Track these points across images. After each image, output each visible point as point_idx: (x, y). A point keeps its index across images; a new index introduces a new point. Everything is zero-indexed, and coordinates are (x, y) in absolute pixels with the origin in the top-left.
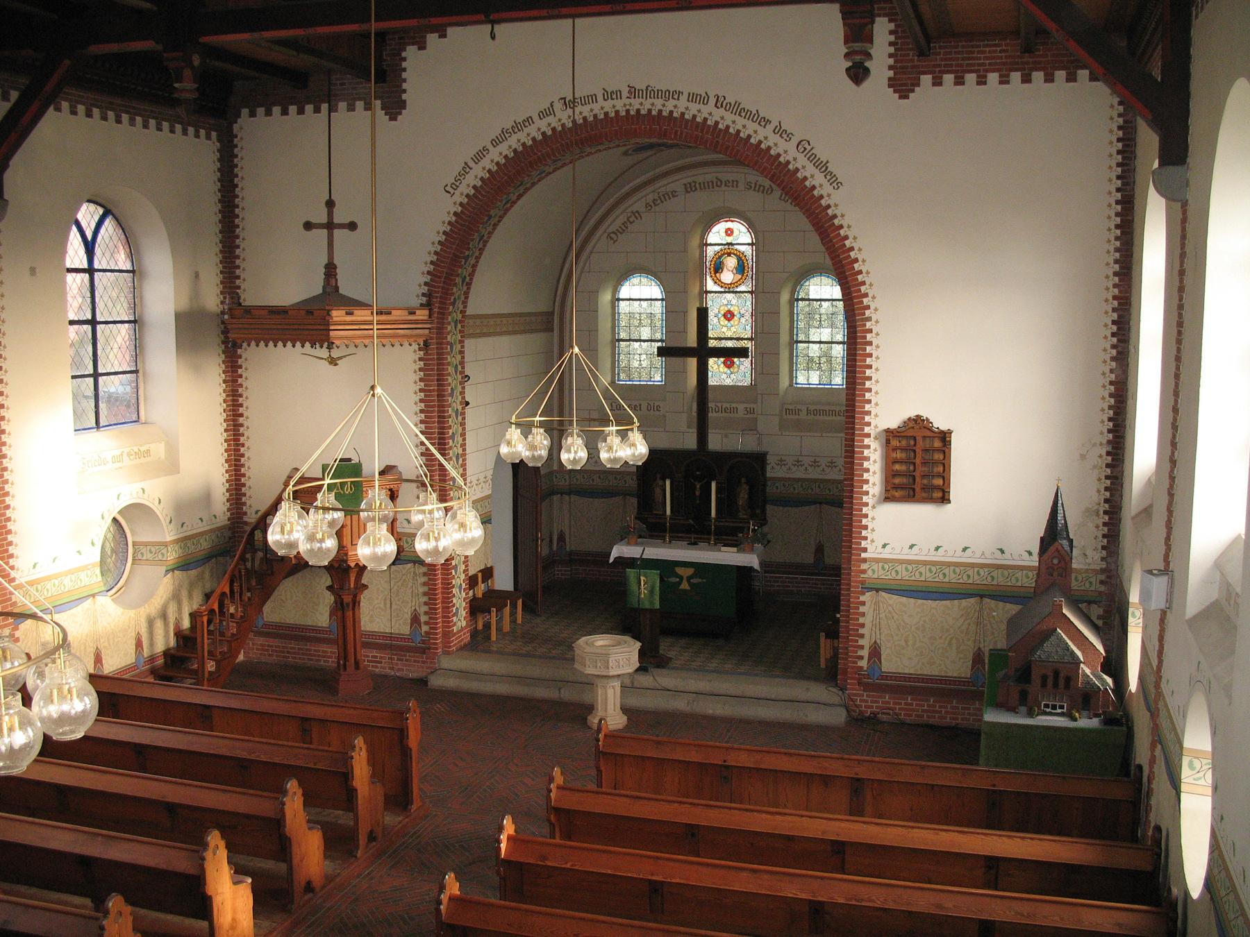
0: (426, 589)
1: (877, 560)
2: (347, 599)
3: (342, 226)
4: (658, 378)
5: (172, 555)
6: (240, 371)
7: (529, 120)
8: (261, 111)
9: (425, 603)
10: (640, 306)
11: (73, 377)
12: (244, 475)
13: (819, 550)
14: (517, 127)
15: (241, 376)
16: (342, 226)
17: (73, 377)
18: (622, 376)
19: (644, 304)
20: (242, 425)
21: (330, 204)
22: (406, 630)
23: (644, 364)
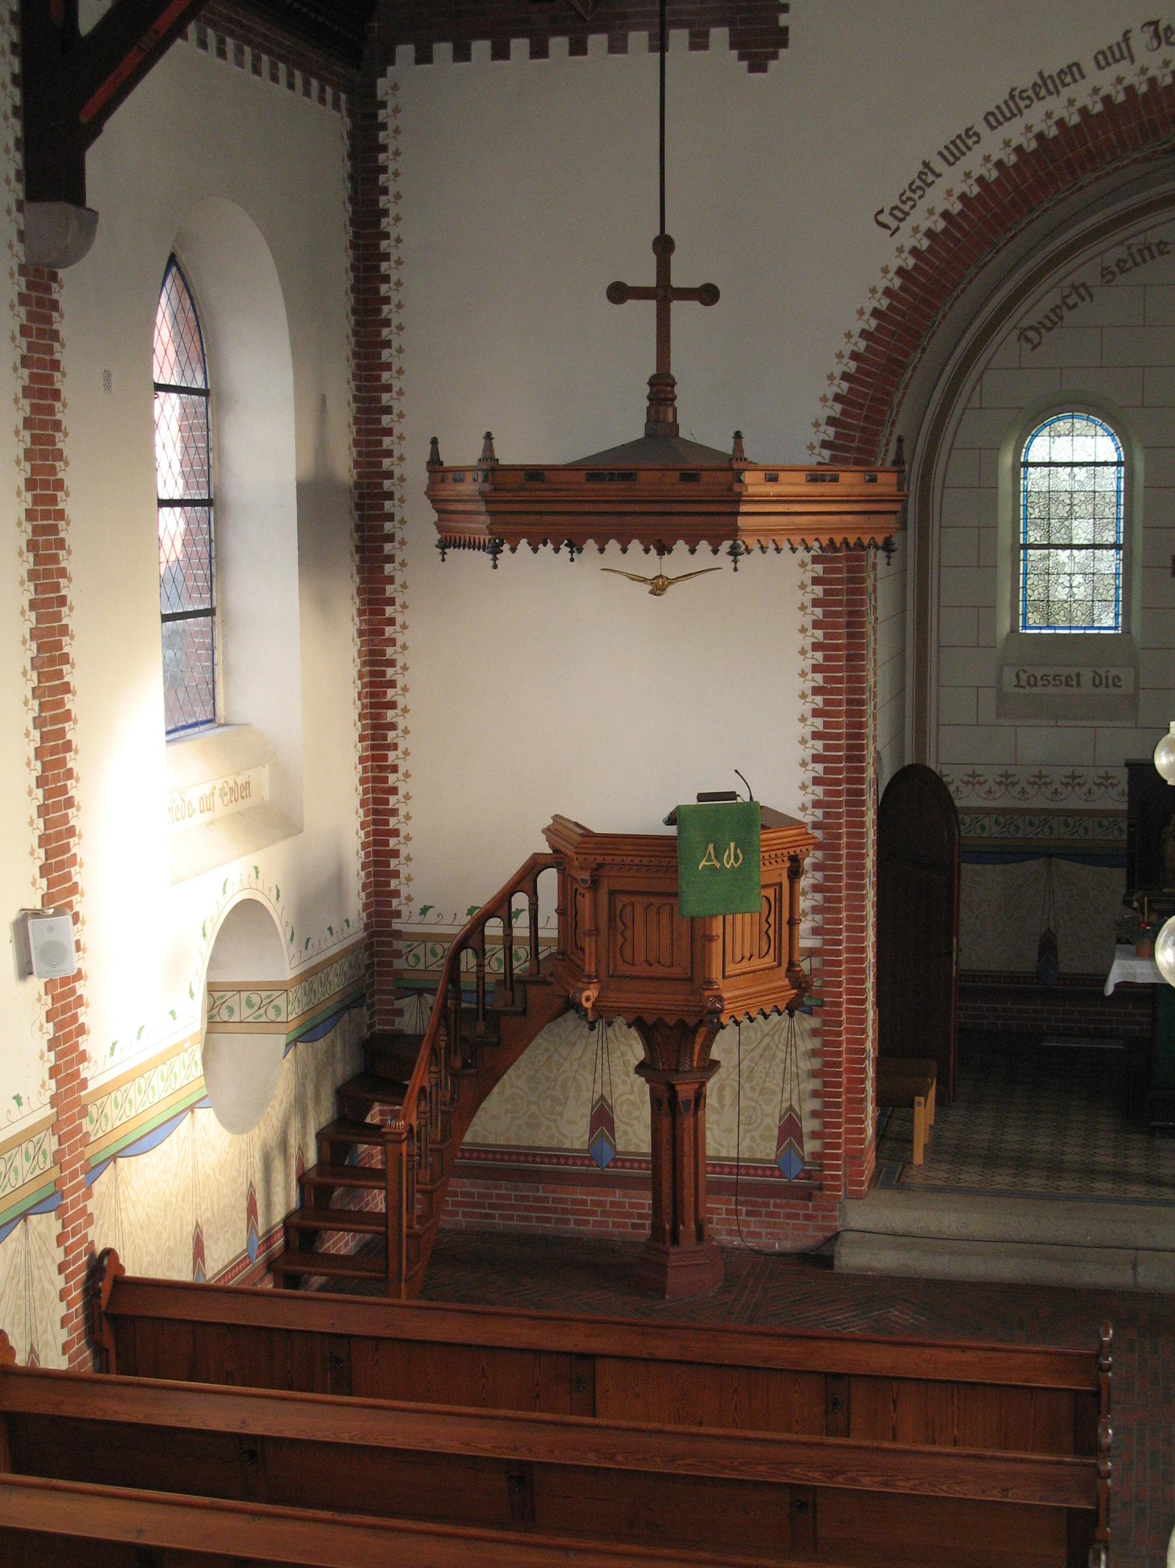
0: (817, 1063)
1: (412, 936)
2: (685, 1091)
3: (642, 293)
4: (1107, 619)
5: (290, 1010)
6: (389, 611)
7: (1073, 71)
8: (443, 50)
9: (815, 1094)
10: (1072, 476)
11: (166, 618)
12: (396, 833)
13: (1048, 945)
14: (1046, 85)
15: (391, 622)
16: (642, 293)
17: (166, 618)
18: (1033, 618)
19: (1081, 473)
20: (393, 726)
21: (664, 246)
22: (765, 1148)
23: (1080, 593)
